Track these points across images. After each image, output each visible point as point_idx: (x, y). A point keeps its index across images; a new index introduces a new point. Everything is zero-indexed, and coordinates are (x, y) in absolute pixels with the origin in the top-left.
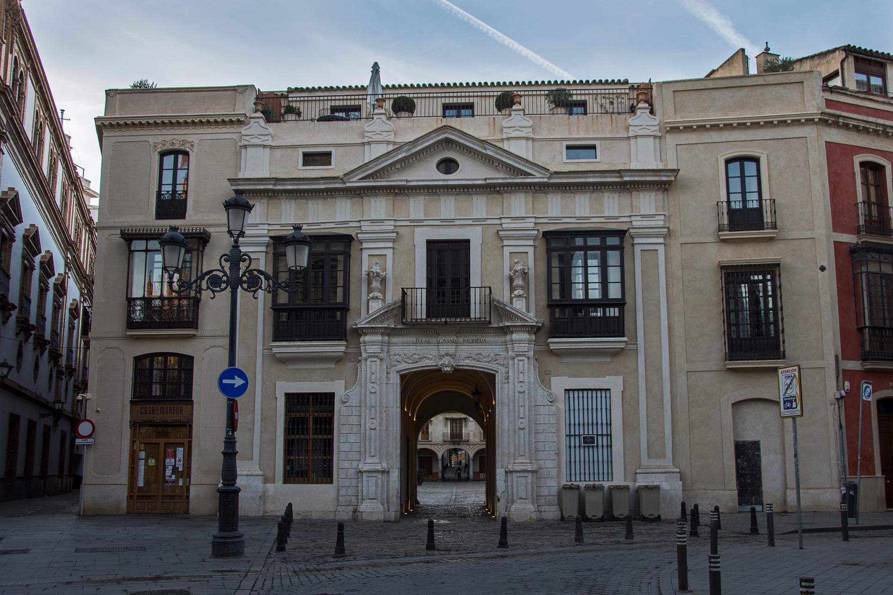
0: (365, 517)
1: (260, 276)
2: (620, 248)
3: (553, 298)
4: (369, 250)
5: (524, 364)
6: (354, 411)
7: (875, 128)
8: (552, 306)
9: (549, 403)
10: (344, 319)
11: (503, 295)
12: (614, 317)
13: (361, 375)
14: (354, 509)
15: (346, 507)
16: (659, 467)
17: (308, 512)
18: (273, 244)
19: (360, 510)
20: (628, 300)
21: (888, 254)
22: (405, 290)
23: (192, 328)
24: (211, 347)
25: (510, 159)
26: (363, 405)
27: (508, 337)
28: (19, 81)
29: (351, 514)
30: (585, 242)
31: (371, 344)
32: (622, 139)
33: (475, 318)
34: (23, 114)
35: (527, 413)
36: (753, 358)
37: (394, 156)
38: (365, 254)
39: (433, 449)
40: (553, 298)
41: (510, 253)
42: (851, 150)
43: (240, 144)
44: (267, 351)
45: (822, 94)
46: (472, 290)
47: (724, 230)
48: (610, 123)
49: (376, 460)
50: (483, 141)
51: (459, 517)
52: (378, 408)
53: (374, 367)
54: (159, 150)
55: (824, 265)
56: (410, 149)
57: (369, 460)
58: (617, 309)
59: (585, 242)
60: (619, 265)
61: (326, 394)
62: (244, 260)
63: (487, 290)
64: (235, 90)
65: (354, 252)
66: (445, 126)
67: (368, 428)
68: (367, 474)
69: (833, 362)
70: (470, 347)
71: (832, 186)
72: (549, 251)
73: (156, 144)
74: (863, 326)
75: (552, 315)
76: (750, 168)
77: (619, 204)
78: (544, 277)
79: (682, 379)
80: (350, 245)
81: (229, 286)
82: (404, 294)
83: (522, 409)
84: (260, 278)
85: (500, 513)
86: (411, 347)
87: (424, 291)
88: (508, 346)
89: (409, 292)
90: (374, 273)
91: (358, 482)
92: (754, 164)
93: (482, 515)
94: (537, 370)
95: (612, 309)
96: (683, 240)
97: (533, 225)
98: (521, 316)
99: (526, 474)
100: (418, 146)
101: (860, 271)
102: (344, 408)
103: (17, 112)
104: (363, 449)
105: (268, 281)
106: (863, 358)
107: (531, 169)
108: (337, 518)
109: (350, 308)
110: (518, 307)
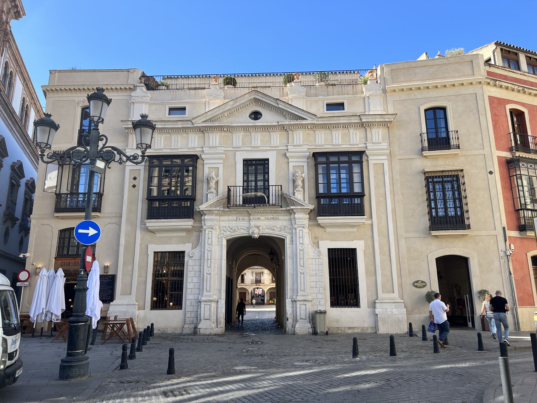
0: (202, 331)
1: (114, 152)
2: (360, 163)
3: (320, 192)
4: (208, 165)
6: (197, 263)
7: (517, 88)
8: (319, 197)
10: (192, 205)
11: (288, 190)
13: (202, 239)
14: (195, 326)
15: (189, 325)
16: (390, 299)
17: (165, 329)
18: (149, 160)
19: (199, 327)
20: (366, 192)
21: (532, 164)
22: (230, 187)
23: (97, 212)
24: (108, 223)
25: (293, 110)
26: (202, 259)
28: (8, 76)
29: (192, 330)
30: (339, 159)
31: (209, 220)
33: (272, 204)
34: (12, 96)
36: (449, 229)
39: (246, 288)
40: (320, 192)
41: (293, 166)
42: (503, 102)
43: (130, 102)
44: (144, 226)
45: (484, 68)
46: (271, 187)
47: (425, 150)
48: (352, 89)
50: (277, 99)
51: (262, 330)
54: (81, 105)
55: (492, 171)
58: (359, 199)
59: (339, 159)
60: (360, 172)
61: (180, 252)
62: (102, 140)
64: (129, 71)
65: (199, 166)
68: (204, 303)
69: (502, 232)
70: (269, 222)
71: (494, 123)
72: (316, 166)
73: (79, 102)
74: (520, 208)
75: (319, 203)
76: (440, 113)
78: (313, 181)
79: (402, 243)
80: (197, 162)
81: (89, 159)
82: (229, 190)
84: (113, 153)
85: (288, 329)
86: (233, 223)
87: (241, 188)
88: (292, 221)
89: (232, 189)
90: (211, 178)
91: (198, 308)
92: (442, 111)
93: (276, 329)
94: (310, 236)
95: (356, 199)
96: (400, 157)
97: (306, 150)
98: (300, 203)
101: (515, 174)
103: (3, 90)
104: (201, 287)
105: (120, 155)
106: (521, 229)
107: (306, 115)
108: (184, 332)
109: (196, 199)
110: (299, 198)
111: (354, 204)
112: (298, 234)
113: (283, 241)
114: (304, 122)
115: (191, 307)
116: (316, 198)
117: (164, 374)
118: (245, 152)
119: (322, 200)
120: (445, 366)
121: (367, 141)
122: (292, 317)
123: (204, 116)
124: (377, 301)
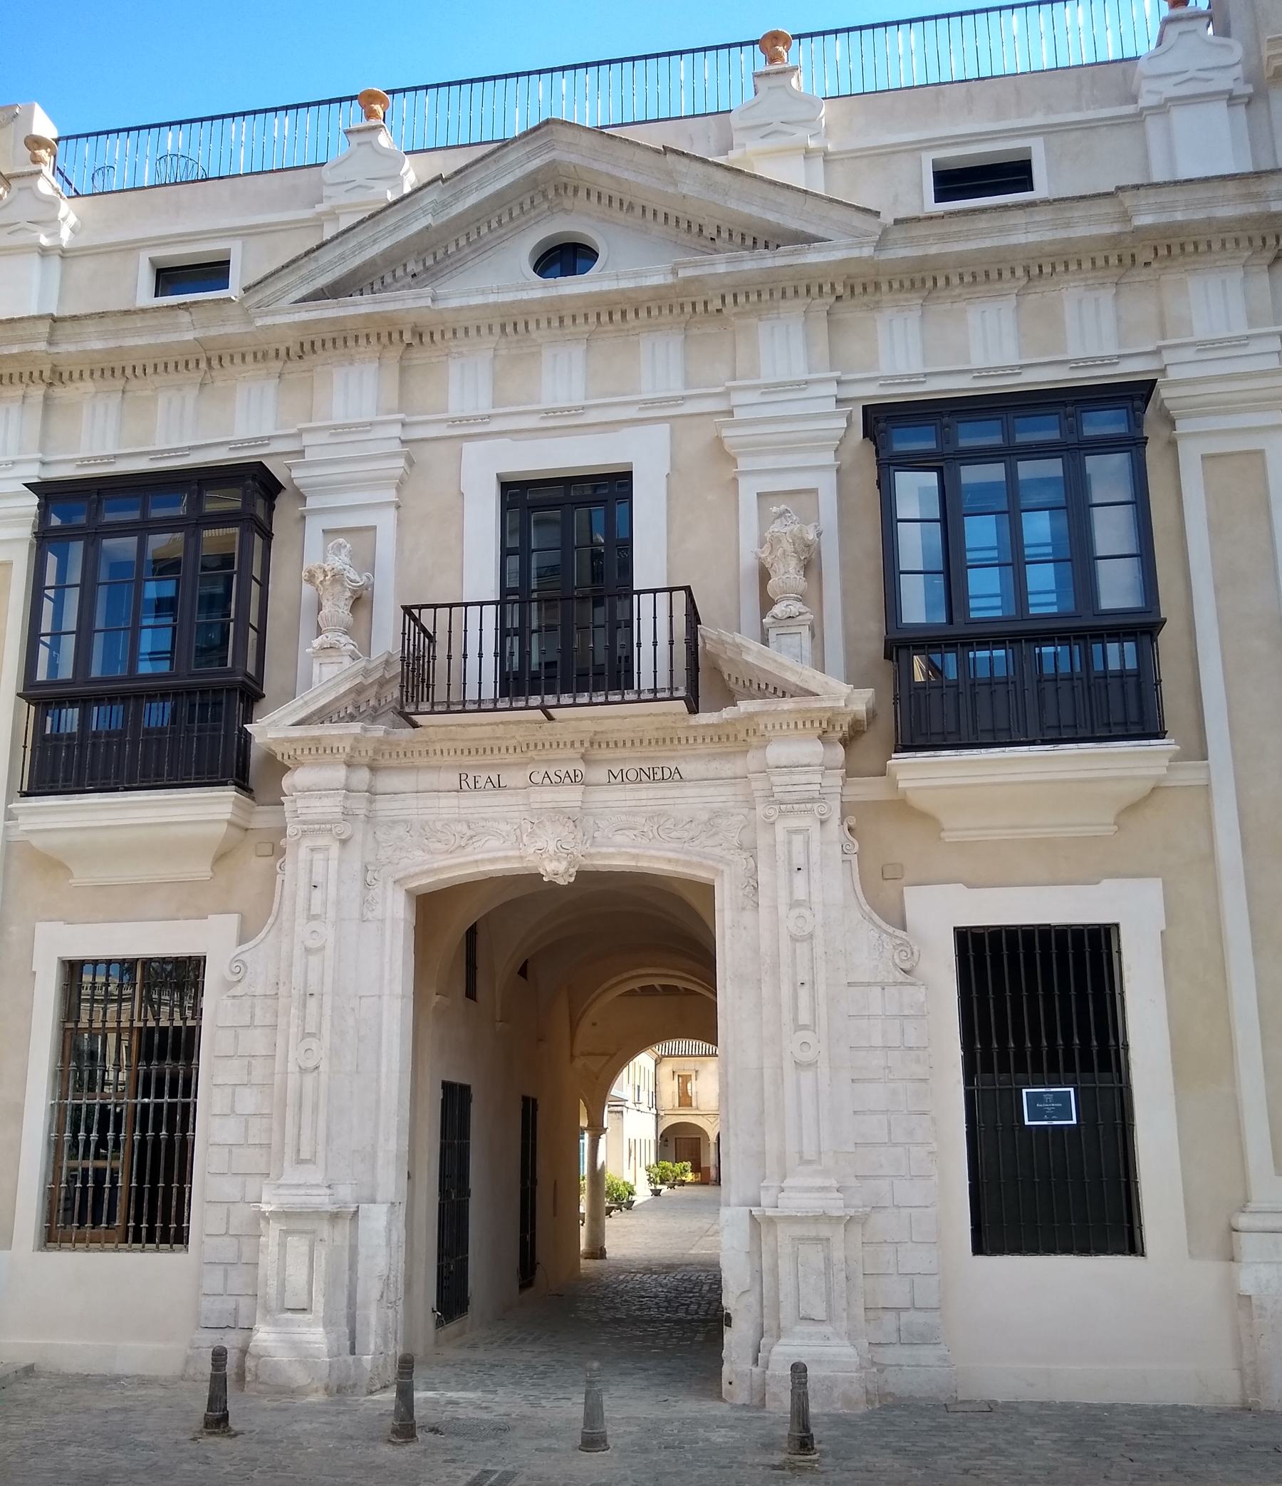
2: (1133, 444)
5: (807, 843)
6: (258, 1012)
9: (900, 977)
12: (1122, 674)
20: (1168, 606)
22: (426, 617)
27: (752, 761)
32: (1115, 123)
35: (822, 1010)
37: (397, 227)
38: (314, 528)
49: (314, 1175)
52: (327, 1000)
53: (319, 867)
56: (446, 205)
57: (292, 1175)
63: (680, 597)
66: (547, 122)
67: (292, 1067)
77: (1119, 319)
83: (804, 994)
88: (754, 785)
94: (855, 862)
95: (1113, 648)
99: (825, 1231)
100: (470, 193)
102: (229, 1002)
111: (1106, 674)
112: (781, 850)
113: (707, 890)
114: (813, 257)
115: (227, 1239)
116: (888, 656)
117: (791, 893)
118: (505, 441)
119: (918, 663)
120: (1009, 1005)
121: (1164, 339)
122: (756, 1308)
123: (304, 271)
124: (1243, 1221)
